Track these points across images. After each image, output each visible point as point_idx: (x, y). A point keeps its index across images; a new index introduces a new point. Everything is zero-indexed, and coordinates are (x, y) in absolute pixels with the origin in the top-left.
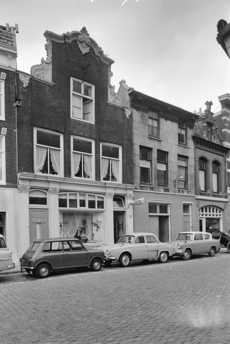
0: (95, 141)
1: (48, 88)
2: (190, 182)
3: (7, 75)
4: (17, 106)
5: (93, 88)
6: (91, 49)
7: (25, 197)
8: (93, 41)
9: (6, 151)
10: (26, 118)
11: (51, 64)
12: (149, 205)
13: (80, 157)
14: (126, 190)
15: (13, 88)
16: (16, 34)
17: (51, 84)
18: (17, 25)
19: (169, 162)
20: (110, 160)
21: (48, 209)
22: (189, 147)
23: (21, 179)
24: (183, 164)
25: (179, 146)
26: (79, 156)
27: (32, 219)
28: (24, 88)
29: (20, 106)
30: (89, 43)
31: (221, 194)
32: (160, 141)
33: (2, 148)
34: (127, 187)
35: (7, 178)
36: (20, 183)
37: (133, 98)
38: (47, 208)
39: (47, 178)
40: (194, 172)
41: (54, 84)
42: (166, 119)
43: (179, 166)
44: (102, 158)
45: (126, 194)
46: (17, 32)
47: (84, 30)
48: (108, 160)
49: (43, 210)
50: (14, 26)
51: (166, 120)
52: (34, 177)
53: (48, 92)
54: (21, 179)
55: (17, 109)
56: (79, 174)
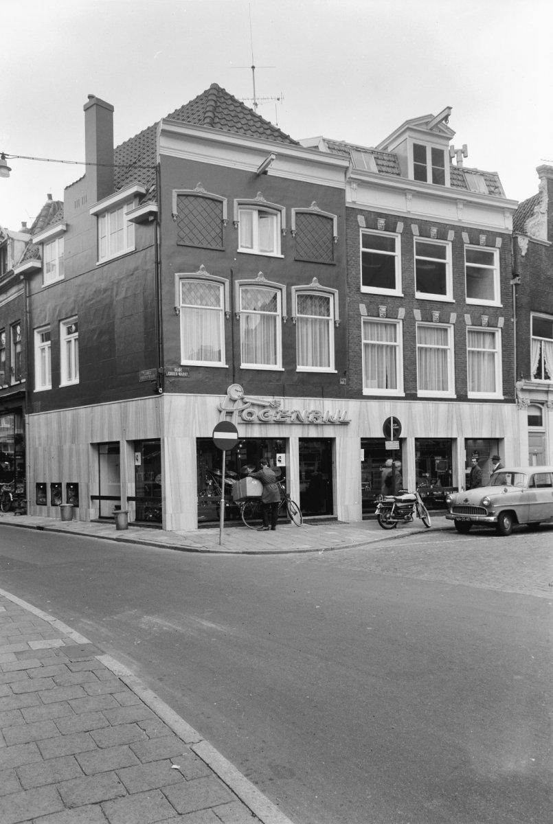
1: (544, 250)
3: (503, 240)
4: (516, 285)
7: (524, 415)
9: (503, 351)
10: (525, 300)
11: (546, 215)
12: (331, 438)
13: (539, 346)
15: (510, 260)
16: (464, 159)
17: (545, 243)
18: (465, 146)
20: (543, 342)
21: (544, 433)
23: (523, 390)
26: (315, 327)
28: (522, 257)
29: (519, 284)
33: (449, 342)
35: (504, 389)
36: (521, 395)
41: (551, 243)
44: (533, 339)
45: (547, 401)
46: (465, 157)
48: (539, 344)
49: (539, 435)
50: (461, 148)
53: (544, 258)
54: (523, 390)
55: (516, 288)
56: (538, 376)
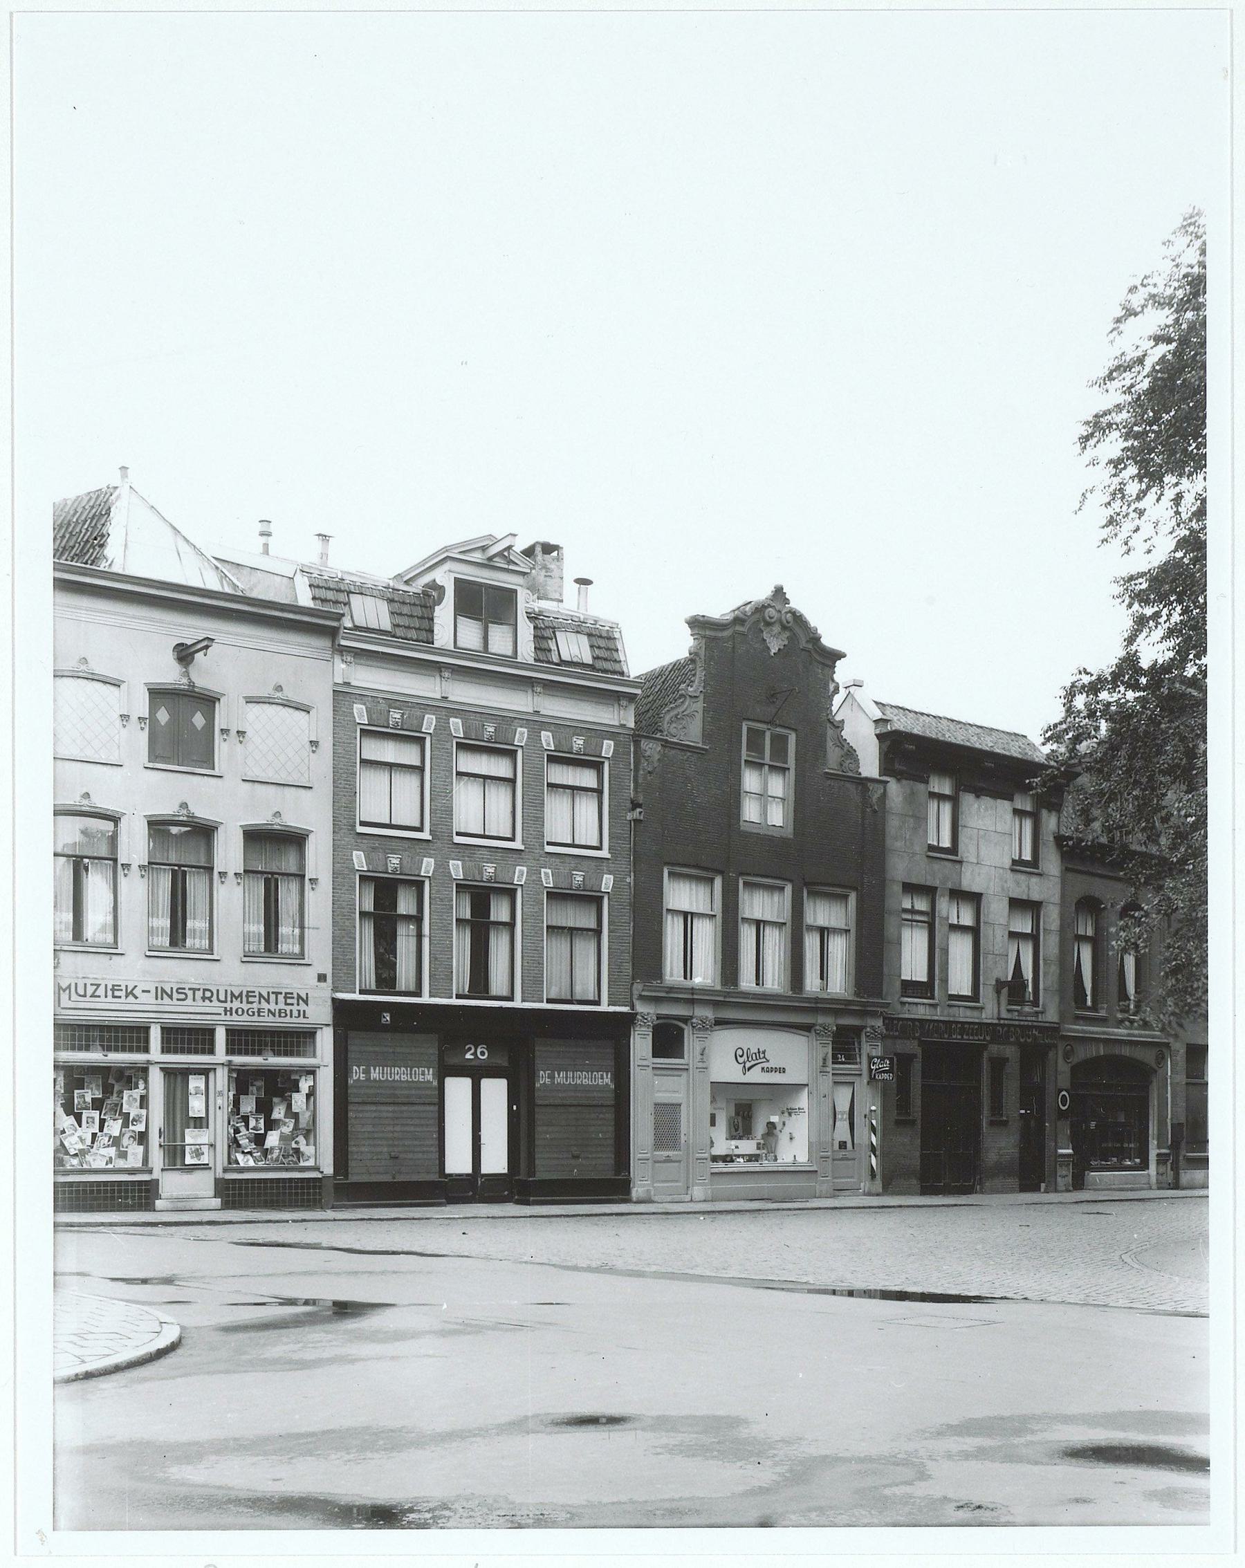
0: (723, 879)
2: (1044, 983)
5: (792, 738)
6: (793, 639)
8: (798, 619)
14: (693, 1004)
19: (982, 924)
22: (1046, 872)
24: (1024, 925)
25: (1012, 870)
27: (656, 1095)
30: (788, 622)
31: (1103, 1013)
32: (960, 862)
34: (695, 997)
37: (889, 747)
38: (686, 1067)
39: (693, 994)
40: (1057, 952)
42: (979, 793)
43: (1013, 935)
45: (692, 1017)
47: (779, 593)
51: (978, 797)
52: (725, 997)
